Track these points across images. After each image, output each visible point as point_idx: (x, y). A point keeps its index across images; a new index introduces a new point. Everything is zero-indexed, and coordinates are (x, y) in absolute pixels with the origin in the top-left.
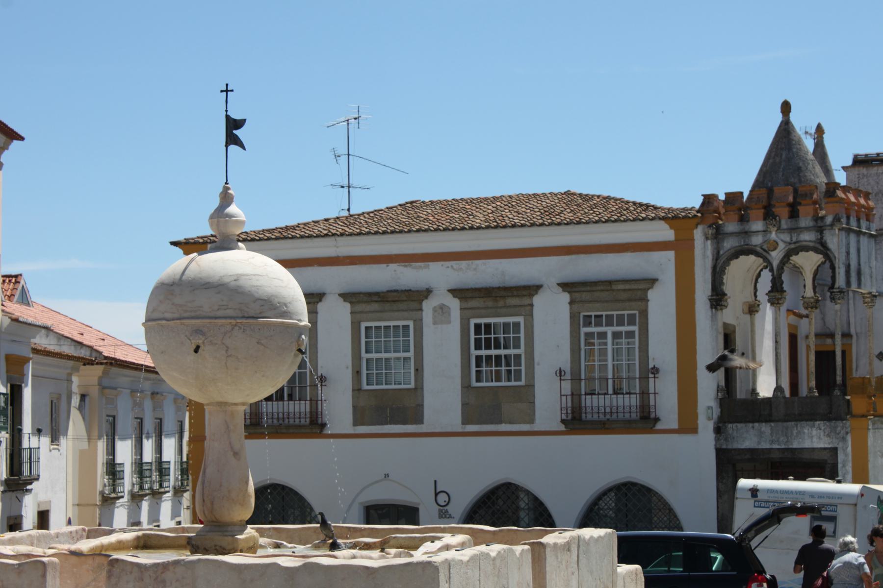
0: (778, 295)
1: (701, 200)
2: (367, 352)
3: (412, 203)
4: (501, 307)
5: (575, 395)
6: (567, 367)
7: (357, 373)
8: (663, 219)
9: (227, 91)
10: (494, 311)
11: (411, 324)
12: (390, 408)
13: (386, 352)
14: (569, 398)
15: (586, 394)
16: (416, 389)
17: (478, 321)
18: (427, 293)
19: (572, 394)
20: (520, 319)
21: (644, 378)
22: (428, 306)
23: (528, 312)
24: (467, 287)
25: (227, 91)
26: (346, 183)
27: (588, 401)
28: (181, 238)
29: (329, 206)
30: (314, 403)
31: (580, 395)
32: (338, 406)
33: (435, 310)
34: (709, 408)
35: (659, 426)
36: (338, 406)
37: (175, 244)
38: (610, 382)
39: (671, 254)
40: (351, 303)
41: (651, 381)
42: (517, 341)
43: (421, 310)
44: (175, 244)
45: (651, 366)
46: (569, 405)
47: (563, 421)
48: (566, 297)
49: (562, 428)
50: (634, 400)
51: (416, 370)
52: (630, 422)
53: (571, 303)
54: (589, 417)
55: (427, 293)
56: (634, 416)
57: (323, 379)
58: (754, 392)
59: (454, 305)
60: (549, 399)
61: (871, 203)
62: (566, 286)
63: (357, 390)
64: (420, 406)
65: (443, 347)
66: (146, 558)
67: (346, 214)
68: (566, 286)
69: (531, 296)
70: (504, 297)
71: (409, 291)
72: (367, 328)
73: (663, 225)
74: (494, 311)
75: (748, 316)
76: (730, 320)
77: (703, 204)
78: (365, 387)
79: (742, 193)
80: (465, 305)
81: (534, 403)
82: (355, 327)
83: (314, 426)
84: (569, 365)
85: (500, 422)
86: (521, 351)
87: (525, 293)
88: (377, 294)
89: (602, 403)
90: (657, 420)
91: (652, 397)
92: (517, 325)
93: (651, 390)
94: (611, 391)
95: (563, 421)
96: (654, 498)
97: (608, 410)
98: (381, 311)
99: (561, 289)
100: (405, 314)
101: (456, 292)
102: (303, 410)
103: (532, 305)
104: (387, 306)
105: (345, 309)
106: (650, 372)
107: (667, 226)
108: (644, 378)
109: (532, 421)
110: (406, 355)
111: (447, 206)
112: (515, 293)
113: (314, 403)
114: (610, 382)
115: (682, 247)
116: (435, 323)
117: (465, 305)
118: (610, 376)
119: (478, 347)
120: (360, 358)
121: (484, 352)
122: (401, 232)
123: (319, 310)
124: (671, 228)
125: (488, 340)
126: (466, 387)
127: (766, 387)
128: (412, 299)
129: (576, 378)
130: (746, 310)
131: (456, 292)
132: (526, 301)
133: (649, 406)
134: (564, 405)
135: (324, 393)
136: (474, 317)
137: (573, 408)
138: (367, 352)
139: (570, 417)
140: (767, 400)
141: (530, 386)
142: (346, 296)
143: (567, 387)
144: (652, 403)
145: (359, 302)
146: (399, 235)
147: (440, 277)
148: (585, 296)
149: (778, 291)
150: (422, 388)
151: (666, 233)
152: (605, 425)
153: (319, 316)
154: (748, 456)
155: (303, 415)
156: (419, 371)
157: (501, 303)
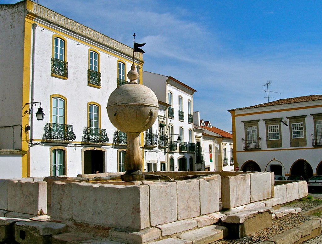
5: (316, 140)
7: (267, 137)
9: (134, 35)
12: (275, 144)
13: (296, 131)
14: (314, 140)
16: (280, 140)
17: (293, 124)
19: (315, 139)
20: (303, 123)
23: (304, 121)
25: (134, 35)
26: (267, 97)
27: (249, 145)
31: (317, 139)
35: (261, 150)
37: (229, 111)
42: (278, 130)
44: (229, 111)
46: (314, 142)
48: (244, 124)
49: (243, 150)
50: (257, 144)
51: (280, 135)
54: (319, 144)
55: (282, 118)
60: (310, 141)
62: (312, 115)
63: (267, 140)
64: (281, 144)
65: (285, 131)
66: (96, 185)
68: (312, 115)
72: (269, 127)
74: (297, 121)
80: (290, 120)
82: (267, 126)
83: (259, 149)
84: (314, 133)
86: (279, 132)
87: (303, 117)
88: (271, 119)
92: (302, 124)
95: (313, 146)
106: (259, 139)
108: (258, 140)
110: (302, 130)
117: (290, 120)
121: (277, 132)
126: (291, 138)
128: (279, 120)
132: (303, 119)
141: (305, 138)
143: (314, 138)
146: (275, 106)
147: (284, 115)
148: (269, 122)
152: (251, 150)
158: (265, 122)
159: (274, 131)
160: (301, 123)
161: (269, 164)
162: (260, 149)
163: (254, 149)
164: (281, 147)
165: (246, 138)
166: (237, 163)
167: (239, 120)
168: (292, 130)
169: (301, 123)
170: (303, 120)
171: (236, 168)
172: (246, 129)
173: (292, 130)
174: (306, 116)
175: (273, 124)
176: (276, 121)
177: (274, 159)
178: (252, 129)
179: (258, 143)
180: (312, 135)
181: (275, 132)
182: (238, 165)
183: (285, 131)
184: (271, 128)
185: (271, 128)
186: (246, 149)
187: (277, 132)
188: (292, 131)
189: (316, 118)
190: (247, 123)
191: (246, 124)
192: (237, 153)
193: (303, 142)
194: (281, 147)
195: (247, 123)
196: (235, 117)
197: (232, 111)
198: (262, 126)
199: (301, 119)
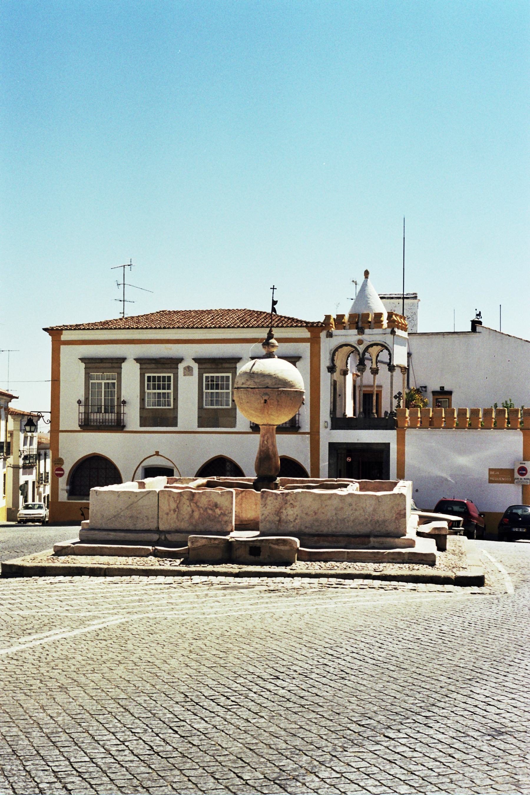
0: (361, 367)
1: (324, 318)
2: (148, 389)
3: (163, 311)
4: (220, 368)
5: (86, 413)
6: (83, 399)
7: (142, 400)
8: (306, 327)
10: (159, 370)
11: (172, 375)
12: (159, 417)
15: (91, 413)
18: (181, 360)
19: (85, 413)
20: (230, 375)
21: (119, 406)
22: (181, 367)
24: (97, 357)
26: (123, 300)
28: (48, 326)
29: (113, 313)
30: (87, 414)
32: (132, 415)
33: (185, 368)
34: (326, 422)
36: (132, 415)
37: (45, 330)
38: (103, 407)
39: (308, 345)
40: (140, 364)
41: (122, 407)
43: (178, 368)
44: (45, 330)
45: (122, 400)
47: (80, 426)
48: (138, 365)
49: (79, 429)
51: (174, 399)
52: (111, 426)
53: (140, 369)
54: (92, 424)
55: (181, 360)
56: (113, 424)
57: (124, 402)
58: (344, 415)
59: (195, 367)
61: (406, 322)
63: (142, 408)
64: (176, 418)
65: (188, 390)
67: (121, 316)
69: (236, 363)
70: (222, 363)
71: (171, 359)
73: (305, 330)
74: (159, 370)
75: (343, 377)
76: (335, 379)
77: (325, 320)
78: (205, 407)
79: (344, 315)
81: (236, 417)
82: (142, 375)
83: (118, 426)
85: (218, 427)
87: (233, 361)
89: (98, 417)
90: (299, 428)
91: (122, 415)
92: (169, 377)
93: (122, 412)
94: (103, 412)
96: (228, 464)
97: (101, 421)
98: (156, 369)
99: (135, 362)
100: (169, 370)
101: (196, 360)
102: (113, 418)
103: (236, 368)
104: (159, 366)
105: (137, 366)
107: (307, 330)
109: (234, 426)
111: (186, 314)
112: (93, 361)
113: (119, 415)
114: (103, 407)
115: (314, 341)
116: (185, 375)
117: (200, 367)
118: (103, 404)
119: (207, 388)
120: (144, 392)
121: (166, 391)
122: (169, 328)
123: (122, 366)
124: (309, 331)
125: (159, 385)
126: (200, 408)
127: (349, 413)
128: (172, 363)
129: (86, 405)
130: (342, 373)
131: (196, 360)
132: (232, 366)
133: (121, 419)
134: (80, 418)
135: (125, 409)
136: (206, 373)
137: (85, 419)
138: (148, 389)
139: (83, 424)
140: (350, 418)
142: (137, 360)
143: (82, 409)
144: (122, 418)
145: (145, 363)
149: (362, 365)
150: (177, 408)
151: (305, 334)
153: (123, 370)
154: (345, 446)
155: (113, 421)
156: (176, 399)
157: (220, 366)
158: (139, 365)
159: (159, 389)
160: (169, 375)
161: (144, 464)
162: (124, 426)
163: (107, 426)
164: (176, 425)
165: (87, 399)
166: (61, 459)
167: (71, 356)
168: (204, 388)
169: (169, 375)
170: (232, 368)
171: (57, 470)
172: (88, 377)
173: (204, 388)
174: (124, 360)
175: (158, 370)
176: (166, 366)
177: (157, 453)
178: (101, 380)
179: (119, 413)
180: (79, 402)
181: (161, 391)
182: (62, 464)
183: (188, 390)
184: (159, 381)
185: (159, 381)
186: (87, 425)
187: (166, 391)
188: (204, 391)
189: (90, 368)
190: (91, 364)
191: (89, 365)
192: (60, 434)
193: (229, 419)
194: (176, 425)
195: (91, 364)
196: (62, 347)
197: (54, 332)
198: (131, 374)
199: (227, 365)
